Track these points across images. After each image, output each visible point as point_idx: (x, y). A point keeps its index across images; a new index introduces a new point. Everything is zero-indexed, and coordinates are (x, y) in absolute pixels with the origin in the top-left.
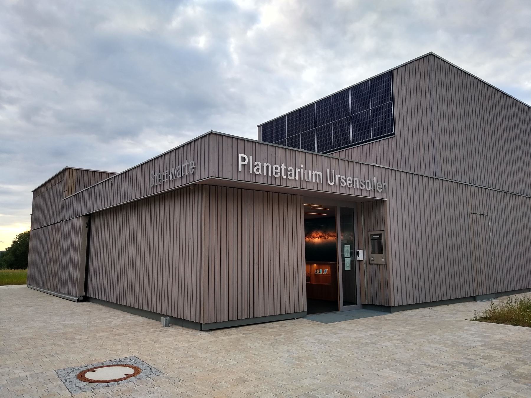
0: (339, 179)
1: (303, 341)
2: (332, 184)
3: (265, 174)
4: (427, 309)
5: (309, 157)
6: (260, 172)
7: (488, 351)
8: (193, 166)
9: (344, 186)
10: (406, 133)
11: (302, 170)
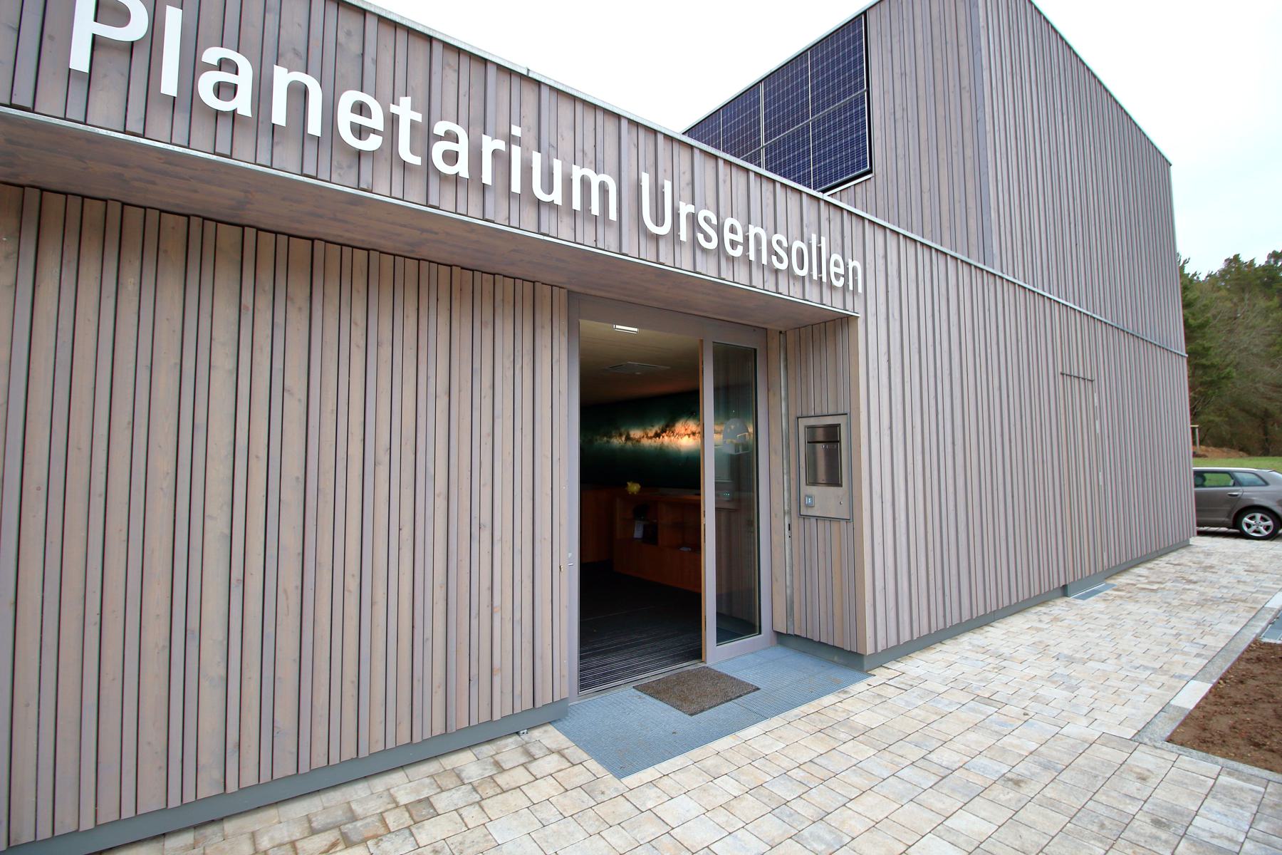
0: (693, 218)
2: (665, 230)
10: (901, 164)
11: (516, 151)
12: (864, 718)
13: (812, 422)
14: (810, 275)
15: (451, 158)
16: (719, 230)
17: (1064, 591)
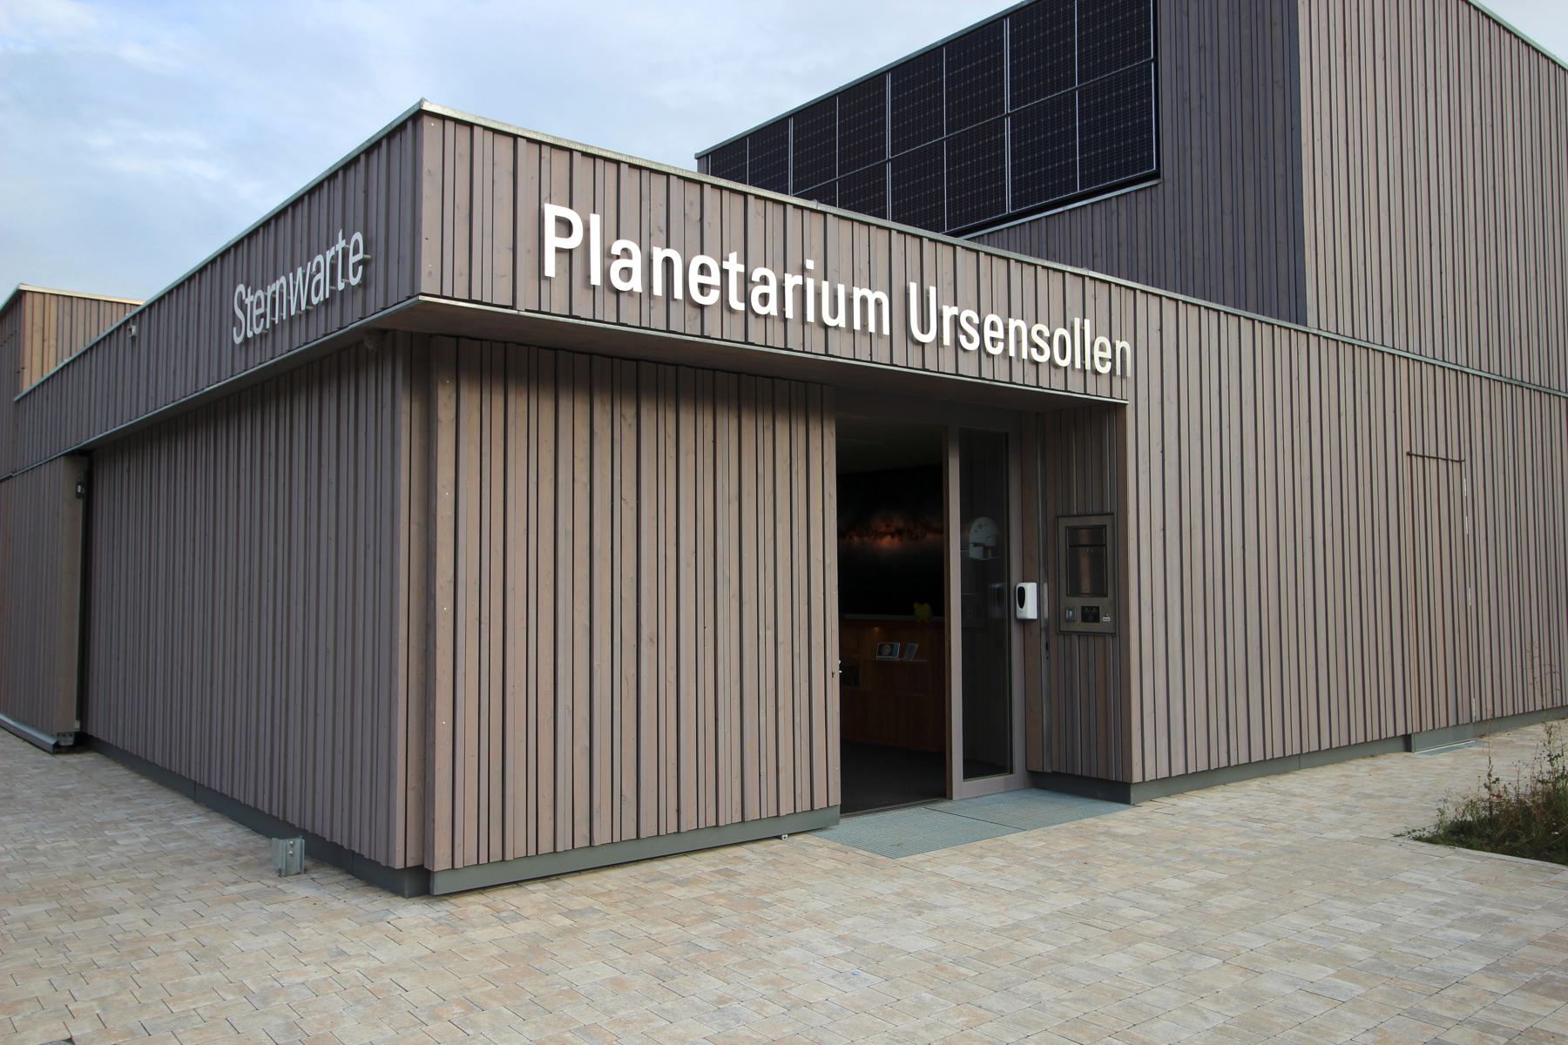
0: (956, 320)
1: (791, 952)
3: (658, 289)
4: (1254, 785)
5: (840, 232)
6: (636, 284)
7: (1520, 1002)
8: (360, 256)
9: (974, 346)
11: (810, 283)
13: (1075, 522)
17: (1407, 743)
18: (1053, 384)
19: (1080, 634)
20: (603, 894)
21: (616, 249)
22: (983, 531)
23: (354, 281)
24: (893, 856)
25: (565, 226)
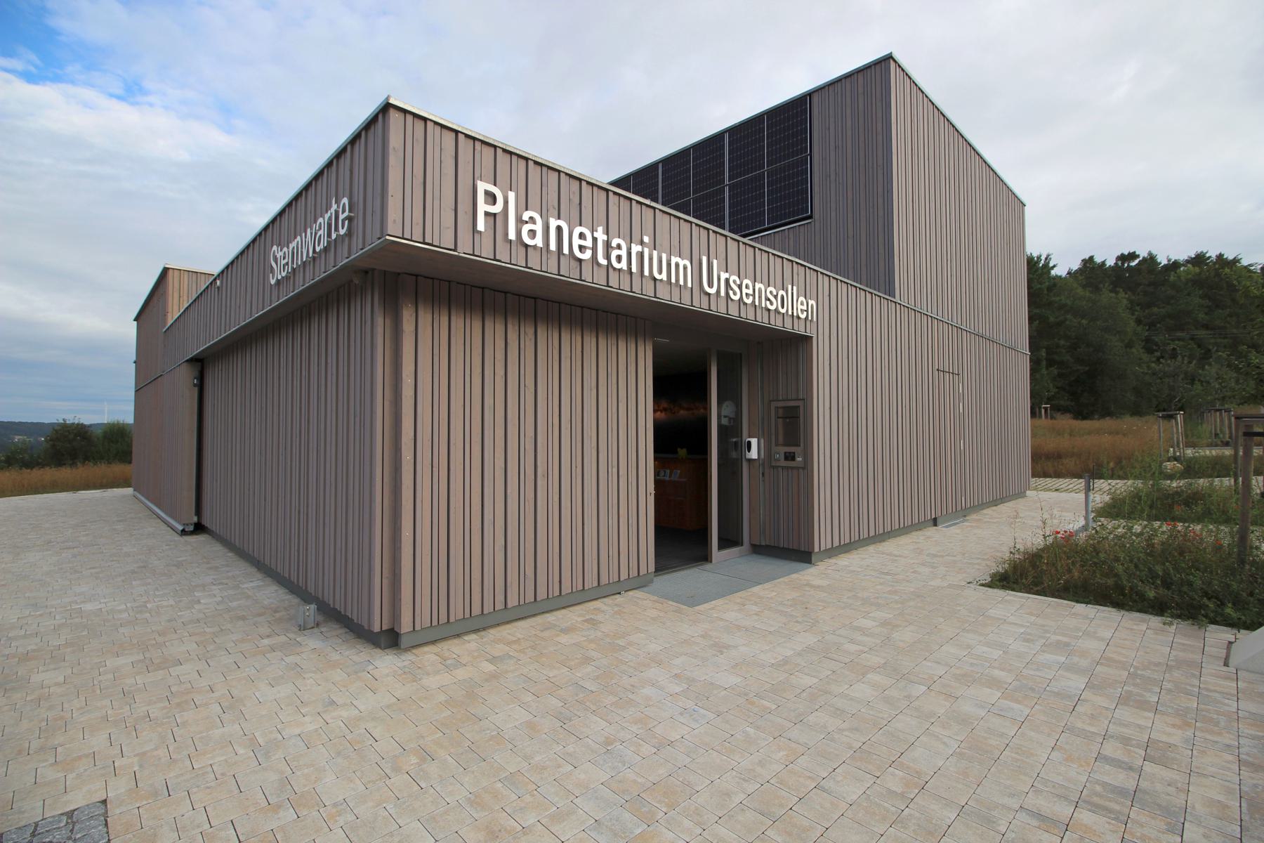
0: (727, 281)
3: (553, 247)
4: (871, 548)
6: (538, 241)
8: (346, 214)
9: (737, 298)
11: (646, 251)
12: (817, 582)
14: (718, 291)
15: (532, 233)
16: (740, 287)
17: (935, 522)
18: (777, 323)
19: (783, 468)
20: (515, 642)
21: (526, 216)
22: (728, 409)
23: (342, 232)
24: (692, 605)
25: (491, 198)
